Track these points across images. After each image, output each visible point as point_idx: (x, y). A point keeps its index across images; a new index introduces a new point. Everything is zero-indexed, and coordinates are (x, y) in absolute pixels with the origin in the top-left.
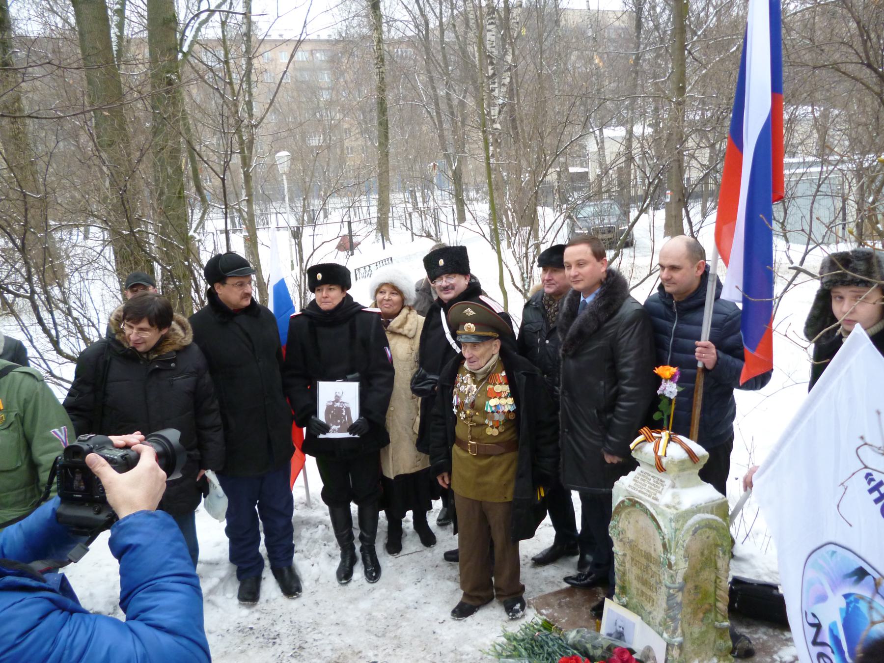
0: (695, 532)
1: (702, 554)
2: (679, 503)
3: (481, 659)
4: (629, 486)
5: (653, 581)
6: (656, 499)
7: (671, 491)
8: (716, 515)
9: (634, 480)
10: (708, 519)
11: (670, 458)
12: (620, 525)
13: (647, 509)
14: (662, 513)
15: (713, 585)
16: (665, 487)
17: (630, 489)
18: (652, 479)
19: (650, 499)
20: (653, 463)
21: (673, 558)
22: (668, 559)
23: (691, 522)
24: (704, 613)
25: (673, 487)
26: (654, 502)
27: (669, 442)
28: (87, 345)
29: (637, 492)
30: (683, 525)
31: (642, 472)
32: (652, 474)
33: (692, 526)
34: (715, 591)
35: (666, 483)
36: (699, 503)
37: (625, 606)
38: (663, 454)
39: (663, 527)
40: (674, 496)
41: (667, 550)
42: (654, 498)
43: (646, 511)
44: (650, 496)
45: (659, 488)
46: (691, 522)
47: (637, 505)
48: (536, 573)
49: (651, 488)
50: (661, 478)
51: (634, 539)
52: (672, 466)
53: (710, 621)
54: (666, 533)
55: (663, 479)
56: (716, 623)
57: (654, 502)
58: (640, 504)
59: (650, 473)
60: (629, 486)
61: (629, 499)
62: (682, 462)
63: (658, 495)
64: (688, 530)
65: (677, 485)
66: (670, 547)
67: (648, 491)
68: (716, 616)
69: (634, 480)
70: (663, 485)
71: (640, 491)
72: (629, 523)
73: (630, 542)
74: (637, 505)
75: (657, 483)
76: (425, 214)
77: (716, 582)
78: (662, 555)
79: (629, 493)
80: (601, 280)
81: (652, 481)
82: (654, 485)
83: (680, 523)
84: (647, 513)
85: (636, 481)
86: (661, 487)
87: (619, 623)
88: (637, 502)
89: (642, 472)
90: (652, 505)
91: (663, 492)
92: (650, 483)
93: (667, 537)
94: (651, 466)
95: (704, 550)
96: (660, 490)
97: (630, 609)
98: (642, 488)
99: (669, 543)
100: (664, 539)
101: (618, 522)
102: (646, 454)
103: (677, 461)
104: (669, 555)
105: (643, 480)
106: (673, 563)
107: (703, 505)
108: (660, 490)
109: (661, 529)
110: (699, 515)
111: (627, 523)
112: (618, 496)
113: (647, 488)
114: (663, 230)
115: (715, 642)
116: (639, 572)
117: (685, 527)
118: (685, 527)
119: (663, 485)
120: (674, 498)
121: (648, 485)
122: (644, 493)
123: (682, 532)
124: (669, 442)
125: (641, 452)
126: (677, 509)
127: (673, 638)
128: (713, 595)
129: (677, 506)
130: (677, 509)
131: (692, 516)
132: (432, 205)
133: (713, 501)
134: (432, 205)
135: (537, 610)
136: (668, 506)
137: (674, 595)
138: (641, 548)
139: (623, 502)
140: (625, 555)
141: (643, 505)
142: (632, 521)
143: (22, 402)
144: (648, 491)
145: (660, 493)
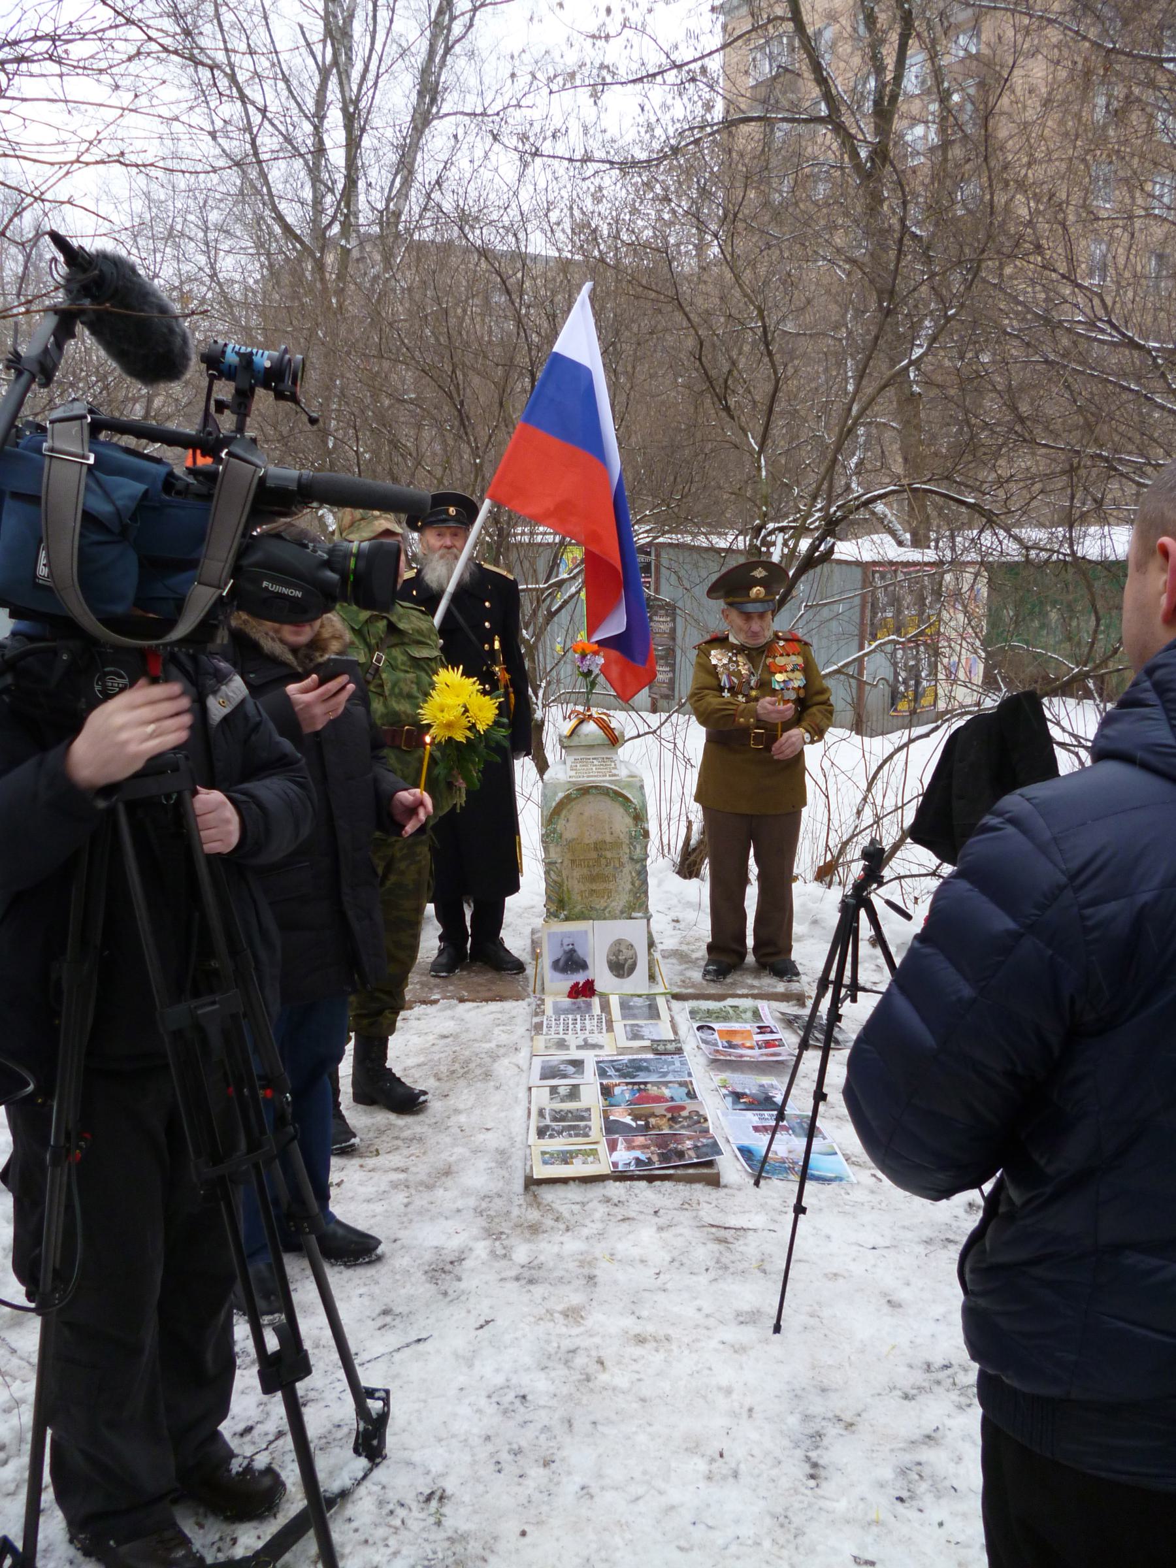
5: (609, 870)
6: (615, 775)
13: (608, 788)
19: (608, 778)
37: (567, 919)
58: (596, 787)
73: (569, 842)
79: (574, 783)
87: (566, 942)
90: (611, 782)
97: (573, 920)
116: (585, 871)
142: (571, 817)
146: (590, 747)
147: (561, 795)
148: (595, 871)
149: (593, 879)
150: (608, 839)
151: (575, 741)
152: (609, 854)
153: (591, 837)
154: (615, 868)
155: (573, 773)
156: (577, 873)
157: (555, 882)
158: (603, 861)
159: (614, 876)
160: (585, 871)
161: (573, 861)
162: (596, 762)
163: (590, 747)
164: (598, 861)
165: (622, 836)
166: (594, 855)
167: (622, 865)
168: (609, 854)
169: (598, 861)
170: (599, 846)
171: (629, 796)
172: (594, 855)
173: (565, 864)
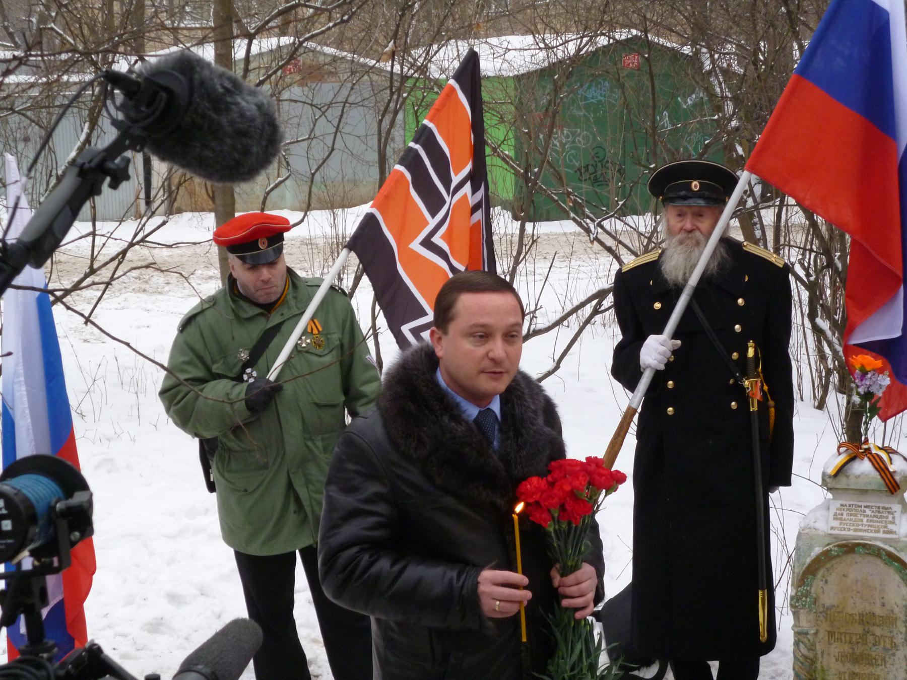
5: (877, 651)
6: (891, 532)
13: (880, 549)
16: (897, 515)
19: (881, 535)
28: (44, 582)
29: (851, 533)
31: (842, 505)
32: (863, 504)
35: (894, 509)
44: (878, 532)
45: (887, 517)
49: (871, 521)
51: (835, 603)
55: (887, 505)
58: (864, 546)
59: (860, 504)
61: (840, 546)
69: (834, 519)
70: (892, 513)
71: (856, 530)
73: (826, 610)
75: (879, 512)
76: (591, 44)
79: (836, 537)
80: (249, 269)
86: (890, 517)
88: (859, 545)
90: (885, 541)
91: (897, 521)
92: (868, 516)
94: (880, 491)
96: (890, 518)
98: (858, 525)
102: (858, 477)
108: (890, 518)
112: (811, 548)
114: (428, 227)
116: (846, 648)
119: (892, 513)
121: (865, 519)
125: (847, 477)
132: (187, 23)
134: (187, 23)
138: (850, 611)
139: (826, 554)
140: (816, 634)
141: (871, 545)
143: (341, 322)
145: (893, 523)
146: (863, 492)
147: (817, 550)
148: (859, 649)
149: (856, 659)
150: (878, 611)
151: (842, 482)
152: (878, 631)
153: (856, 606)
154: (885, 649)
155: (836, 524)
156: (836, 649)
157: (806, 657)
158: (870, 639)
159: (884, 659)
160: (846, 648)
161: (831, 634)
162: (868, 512)
163: (863, 492)
164: (863, 636)
165: (896, 610)
166: (859, 629)
167: (895, 646)
168: (878, 631)
169: (863, 636)
170: (866, 619)
172: (859, 629)
173: (821, 635)
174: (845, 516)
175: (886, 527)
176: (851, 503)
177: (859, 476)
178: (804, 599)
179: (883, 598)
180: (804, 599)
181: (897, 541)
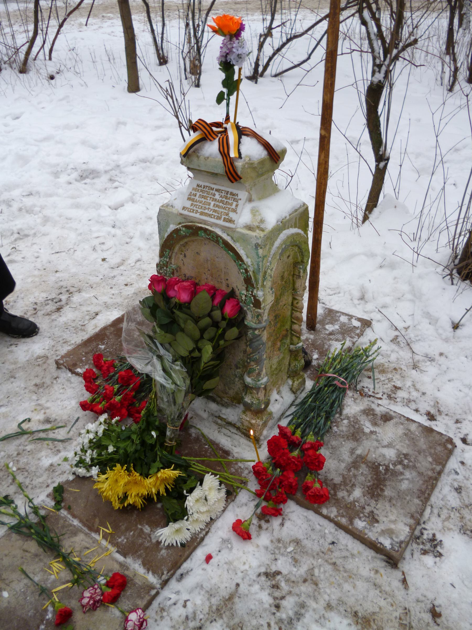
0: (281, 254)
1: (282, 277)
2: (262, 221)
3: (18, 454)
4: (184, 208)
6: (231, 221)
7: (249, 206)
8: (299, 228)
9: (189, 199)
10: (293, 235)
11: (247, 159)
12: (173, 261)
13: (218, 236)
14: (243, 239)
15: (290, 308)
17: (186, 213)
18: (217, 194)
19: (221, 222)
20: (220, 169)
21: (260, 294)
22: (254, 297)
23: (277, 243)
24: (281, 341)
25: (250, 200)
26: (227, 224)
27: (240, 138)
29: (198, 216)
30: (269, 251)
31: (198, 186)
33: (278, 248)
34: (292, 314)
36: (283, 217)
38: (237, 156)
39: (244, 257)
40: (254, 212)
41: (252, 285)
42: (225, 220)
43: (216, 239)
44: (219, 218)
46: (277, 243)
47: (202, 233)
48: (53, 320)
49: (217, 206)
50: (230, 190)
51: (193, 275)
52: (249, 170)
53: (286, 346)
54: (250, 263)
55: (235, 191)
56: (292, 347)
57: (227, 224)
58: (206, 230)
59: (213, 186)
60: (184, 208)
61: (185, 226)
62: (262, 162)
63: (232, 215)
64: (274, 254)
65: (254, 197)
66: (257, 280)
67: (215, 211)
68: (291, 339)
69: (189, 199)
71: (202, 214)
72: (185, 256)
74: (202, 233)
75: (226, 198)
77: (292, 304)
78: (244, 292)
79: (185, 217)
81: (217, 197)
82: (222, 202)
83: (268, 247)
84: (217, 242)
85: (193, 200)
86: (235, 203)
88: (201, 228)
89: (198, 186)
90: (224, 229)
91: (238, 211)
93: (251, 269)
95: (284, 272)
96: (234, 206)
98: (205, 208)
99: (255, 276)
100: (247, 271)
101: (170, 258)
103: (256, 162)
104: (255, 291)
105: (203, 197)
106: (261, 300)
107: (288, 218)
108: (234, 206)
109: (242, 260)
110: (285, 232)
111: (182, 257)
113: (211, 207)
115: (289, 365)
117: (272, 252)
118: (272, 252)
120: (254, 215)
121: (212, 203)
122: (210, 215)
123: (270, 259)
124: (240, 138)
125: (198, 157)
126: (263, 230)
127: (259, 381)
128: (289, 318)
129: (262, 226)
130: (263, 230)
131: (279, 234)
133: (296, 211)
135: (70, 370)
136: (249, 228)
137: (260, 335)
139: (176, 231)
142: (188, 253)
144: (215, 211)
145: (235, 211)
147: (172, 227)
155: (188, 204)
171: (242, 252)
174: (197, 198)
175: (227, 214)
176: (207, 184)
177: (208, 158)
178: (165, 268)
179: (227, 280)
180: (165, 268)
181: (233, 230)
